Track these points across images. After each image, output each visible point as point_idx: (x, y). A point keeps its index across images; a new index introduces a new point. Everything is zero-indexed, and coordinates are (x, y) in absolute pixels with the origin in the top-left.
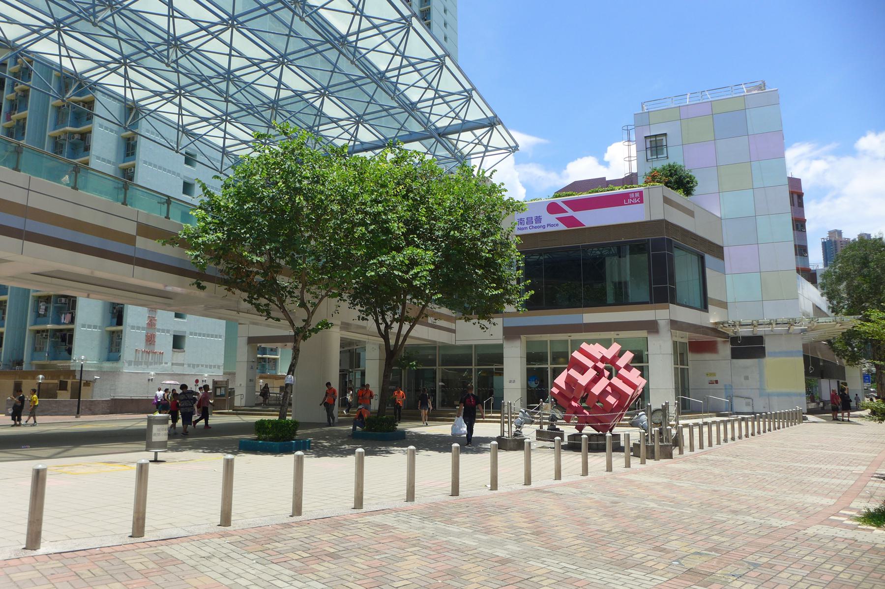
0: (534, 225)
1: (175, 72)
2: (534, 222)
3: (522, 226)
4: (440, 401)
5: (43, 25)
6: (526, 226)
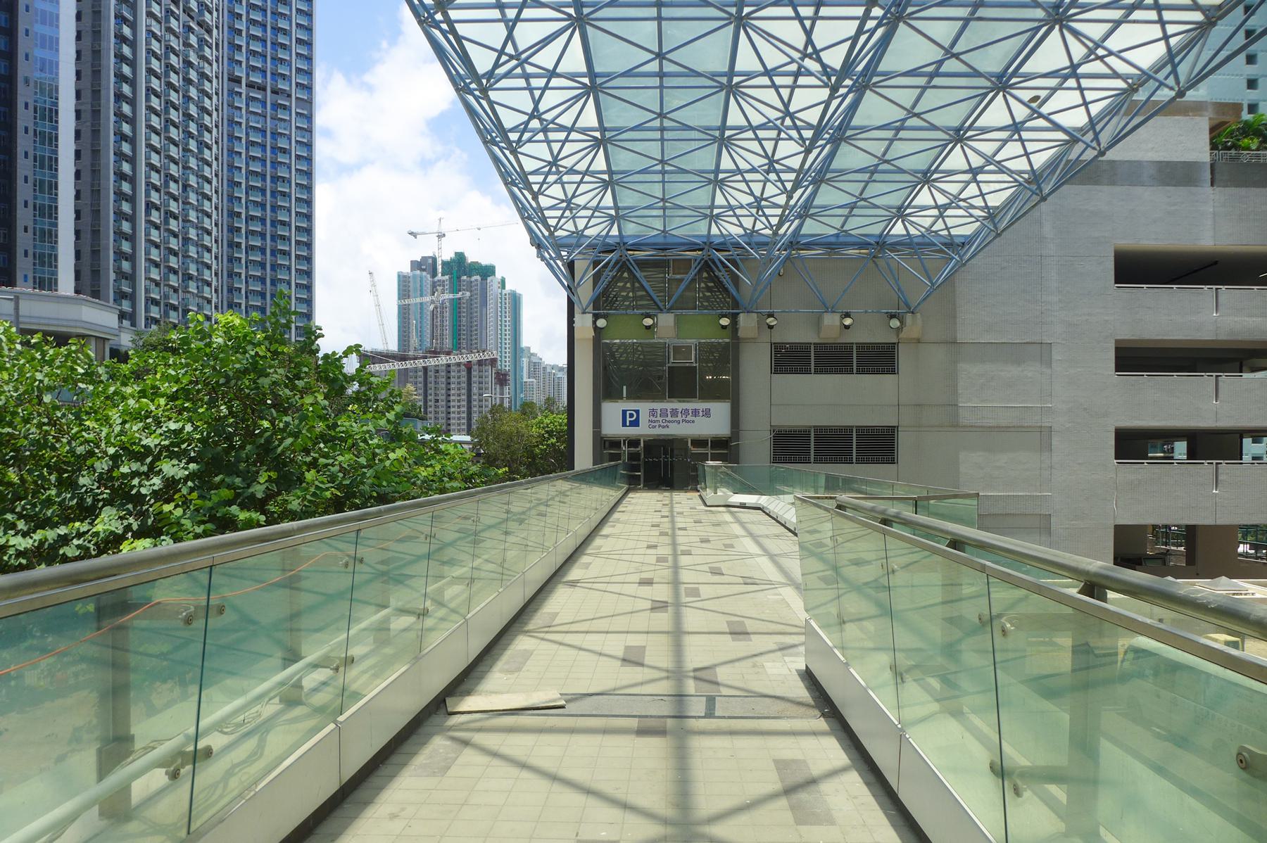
0: (669, 418)
1: (775, 69)
2: (669, 415)
3: (654, 419)
4: (378, 681)
5: (1036, 24)
6: (659, 418)
